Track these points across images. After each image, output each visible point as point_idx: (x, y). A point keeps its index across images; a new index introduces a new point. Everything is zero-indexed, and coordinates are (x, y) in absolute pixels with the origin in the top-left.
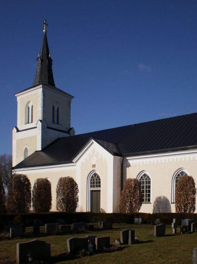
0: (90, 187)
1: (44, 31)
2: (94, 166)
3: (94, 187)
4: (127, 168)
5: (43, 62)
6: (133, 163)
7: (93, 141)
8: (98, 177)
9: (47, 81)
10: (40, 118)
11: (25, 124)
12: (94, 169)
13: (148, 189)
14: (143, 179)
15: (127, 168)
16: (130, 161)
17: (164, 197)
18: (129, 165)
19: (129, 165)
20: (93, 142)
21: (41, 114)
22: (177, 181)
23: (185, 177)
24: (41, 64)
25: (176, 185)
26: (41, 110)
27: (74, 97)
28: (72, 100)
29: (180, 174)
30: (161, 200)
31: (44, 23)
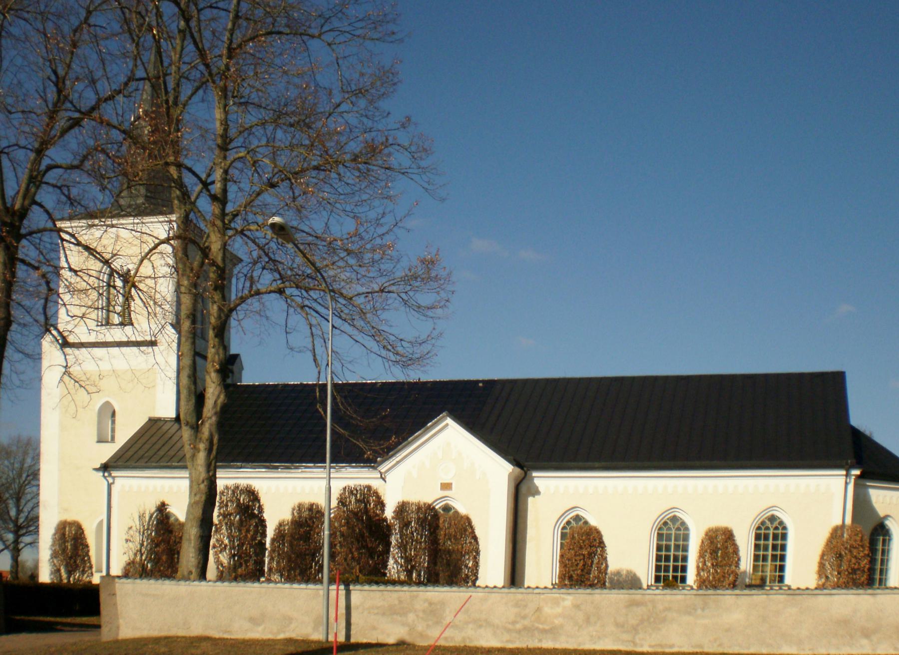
2: (446, 486)
4: (531, 500)
13: (761, 553)
14: (669, 529)
15: (531, 500)
16: (537, 482)
17: (629, 572)
18: (536, 492)
19: (536, 492)
22: (563, 536)
23: (146, 524)
25: (562, 544)
29: (572, 521)
30: (621, 579)
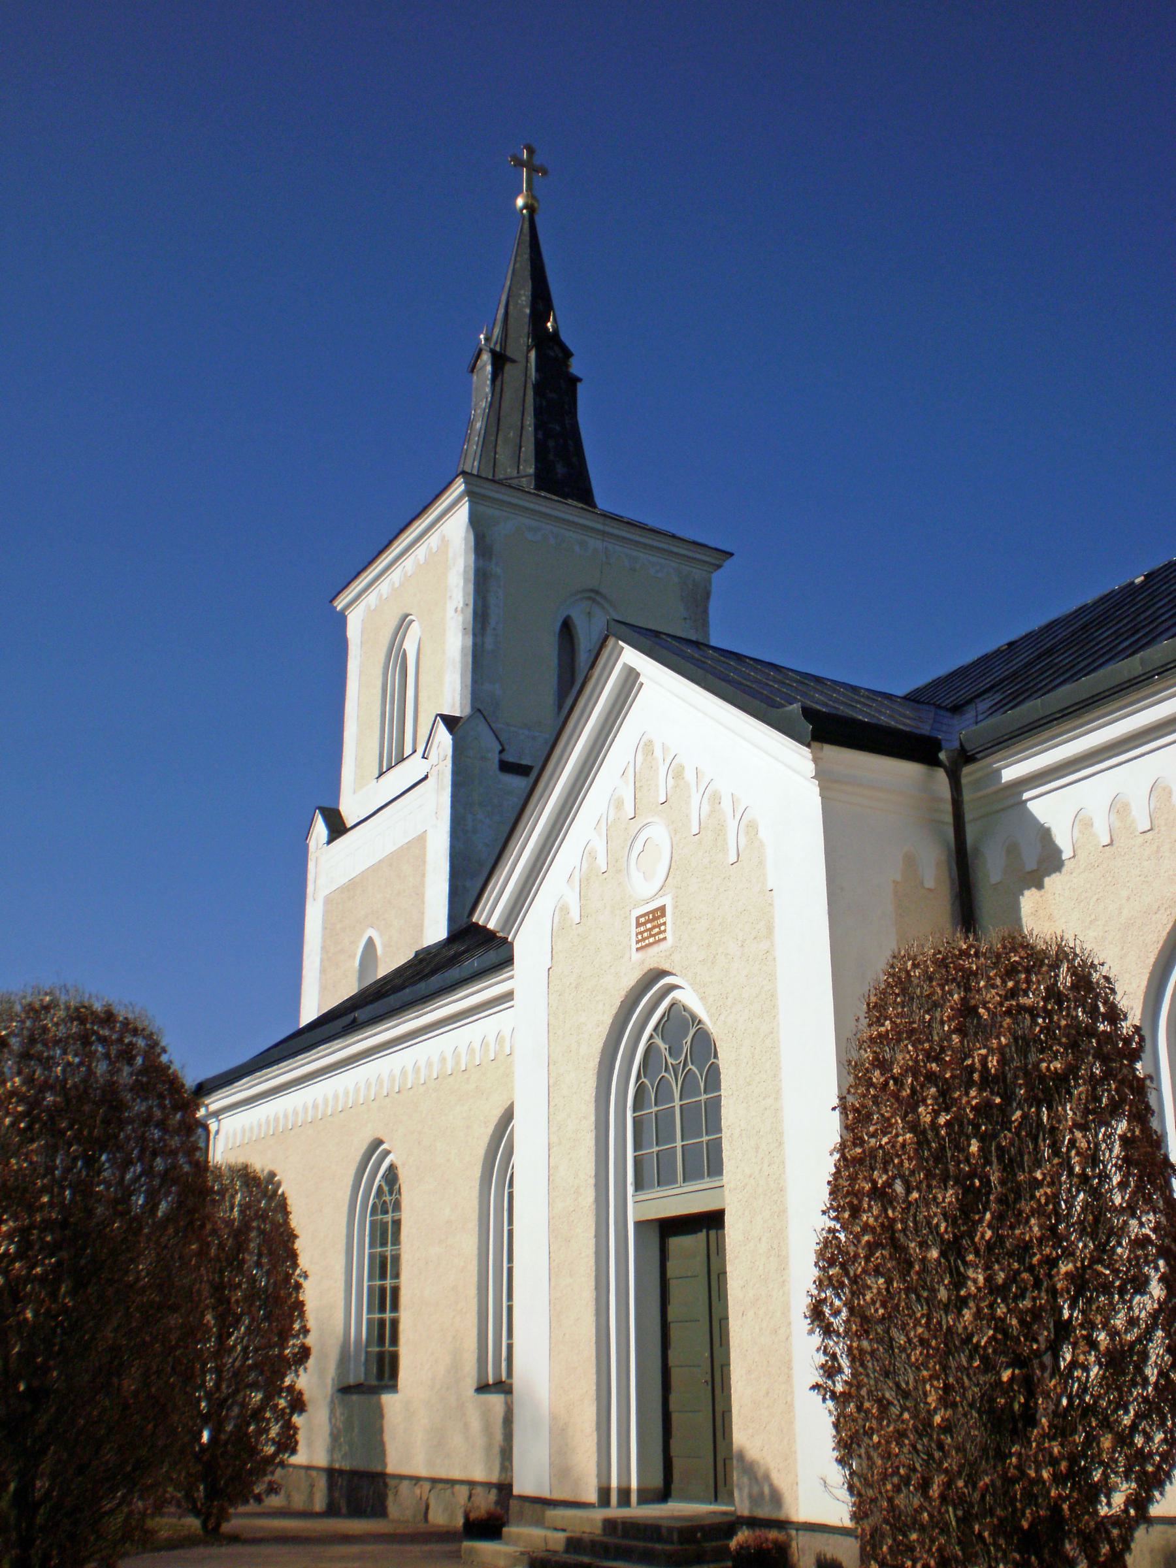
0: (639, 1186)
1: (520, 202)
3: (665, 1178)
5: (508, 367)
6: (1081, 821)
7: (630, 656)
8: (704, 1045)
9: (531, 471)
10: (453, 706)
11: (381, 774)
12: (654, 958)
20: (631, 677)
21: (463, 676)
24: (494, 380)
26: (463, 648)
27: (732, 555)
28: (718, 577)
31: (520, 163)
